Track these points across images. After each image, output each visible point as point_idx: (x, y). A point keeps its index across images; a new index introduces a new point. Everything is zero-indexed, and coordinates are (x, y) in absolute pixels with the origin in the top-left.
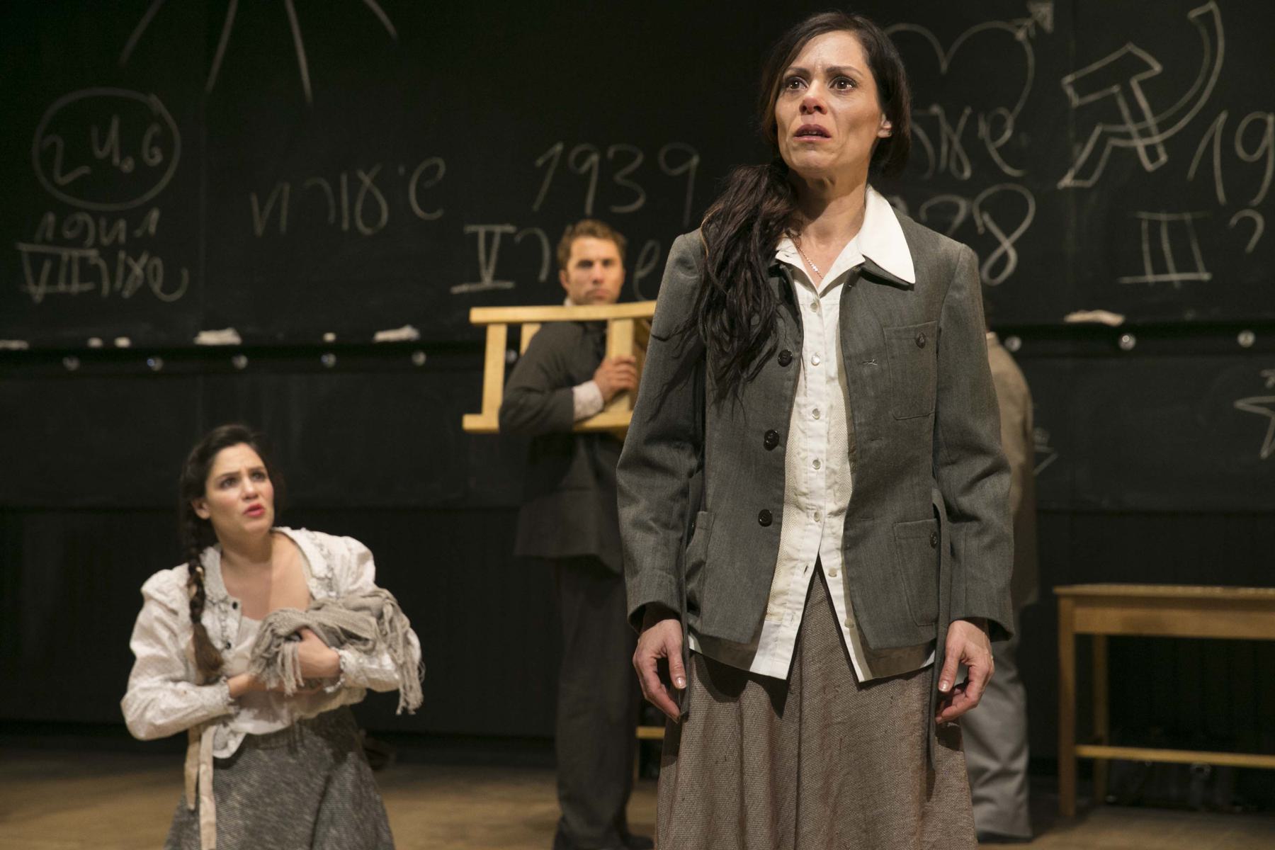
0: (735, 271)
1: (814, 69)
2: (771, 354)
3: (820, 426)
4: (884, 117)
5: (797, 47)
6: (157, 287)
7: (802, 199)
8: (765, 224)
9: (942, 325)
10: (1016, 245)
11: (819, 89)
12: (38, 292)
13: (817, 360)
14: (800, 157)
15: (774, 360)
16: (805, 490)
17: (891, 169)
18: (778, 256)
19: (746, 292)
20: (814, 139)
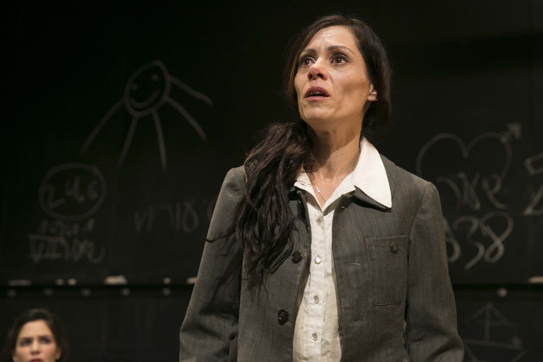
0: (264, 195)
1: (320, 49)
2: (288, 254)
3: (318, 308)
4: (372, 86)
5: (308, 37)
6: (90, 256)
7: (313, 147)
8: (287, 162)
9: (411, 238)
10: (504, 242)
11: (321, 63)
12: (37, 257)
13: (318, 260)
14: (310, 111)
15: (289, 260)
16: (305, 355)
17: (379, 126)
18: (297, 184)
19: (271, 209)
20: (318, 98)
